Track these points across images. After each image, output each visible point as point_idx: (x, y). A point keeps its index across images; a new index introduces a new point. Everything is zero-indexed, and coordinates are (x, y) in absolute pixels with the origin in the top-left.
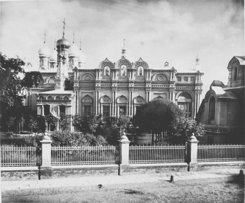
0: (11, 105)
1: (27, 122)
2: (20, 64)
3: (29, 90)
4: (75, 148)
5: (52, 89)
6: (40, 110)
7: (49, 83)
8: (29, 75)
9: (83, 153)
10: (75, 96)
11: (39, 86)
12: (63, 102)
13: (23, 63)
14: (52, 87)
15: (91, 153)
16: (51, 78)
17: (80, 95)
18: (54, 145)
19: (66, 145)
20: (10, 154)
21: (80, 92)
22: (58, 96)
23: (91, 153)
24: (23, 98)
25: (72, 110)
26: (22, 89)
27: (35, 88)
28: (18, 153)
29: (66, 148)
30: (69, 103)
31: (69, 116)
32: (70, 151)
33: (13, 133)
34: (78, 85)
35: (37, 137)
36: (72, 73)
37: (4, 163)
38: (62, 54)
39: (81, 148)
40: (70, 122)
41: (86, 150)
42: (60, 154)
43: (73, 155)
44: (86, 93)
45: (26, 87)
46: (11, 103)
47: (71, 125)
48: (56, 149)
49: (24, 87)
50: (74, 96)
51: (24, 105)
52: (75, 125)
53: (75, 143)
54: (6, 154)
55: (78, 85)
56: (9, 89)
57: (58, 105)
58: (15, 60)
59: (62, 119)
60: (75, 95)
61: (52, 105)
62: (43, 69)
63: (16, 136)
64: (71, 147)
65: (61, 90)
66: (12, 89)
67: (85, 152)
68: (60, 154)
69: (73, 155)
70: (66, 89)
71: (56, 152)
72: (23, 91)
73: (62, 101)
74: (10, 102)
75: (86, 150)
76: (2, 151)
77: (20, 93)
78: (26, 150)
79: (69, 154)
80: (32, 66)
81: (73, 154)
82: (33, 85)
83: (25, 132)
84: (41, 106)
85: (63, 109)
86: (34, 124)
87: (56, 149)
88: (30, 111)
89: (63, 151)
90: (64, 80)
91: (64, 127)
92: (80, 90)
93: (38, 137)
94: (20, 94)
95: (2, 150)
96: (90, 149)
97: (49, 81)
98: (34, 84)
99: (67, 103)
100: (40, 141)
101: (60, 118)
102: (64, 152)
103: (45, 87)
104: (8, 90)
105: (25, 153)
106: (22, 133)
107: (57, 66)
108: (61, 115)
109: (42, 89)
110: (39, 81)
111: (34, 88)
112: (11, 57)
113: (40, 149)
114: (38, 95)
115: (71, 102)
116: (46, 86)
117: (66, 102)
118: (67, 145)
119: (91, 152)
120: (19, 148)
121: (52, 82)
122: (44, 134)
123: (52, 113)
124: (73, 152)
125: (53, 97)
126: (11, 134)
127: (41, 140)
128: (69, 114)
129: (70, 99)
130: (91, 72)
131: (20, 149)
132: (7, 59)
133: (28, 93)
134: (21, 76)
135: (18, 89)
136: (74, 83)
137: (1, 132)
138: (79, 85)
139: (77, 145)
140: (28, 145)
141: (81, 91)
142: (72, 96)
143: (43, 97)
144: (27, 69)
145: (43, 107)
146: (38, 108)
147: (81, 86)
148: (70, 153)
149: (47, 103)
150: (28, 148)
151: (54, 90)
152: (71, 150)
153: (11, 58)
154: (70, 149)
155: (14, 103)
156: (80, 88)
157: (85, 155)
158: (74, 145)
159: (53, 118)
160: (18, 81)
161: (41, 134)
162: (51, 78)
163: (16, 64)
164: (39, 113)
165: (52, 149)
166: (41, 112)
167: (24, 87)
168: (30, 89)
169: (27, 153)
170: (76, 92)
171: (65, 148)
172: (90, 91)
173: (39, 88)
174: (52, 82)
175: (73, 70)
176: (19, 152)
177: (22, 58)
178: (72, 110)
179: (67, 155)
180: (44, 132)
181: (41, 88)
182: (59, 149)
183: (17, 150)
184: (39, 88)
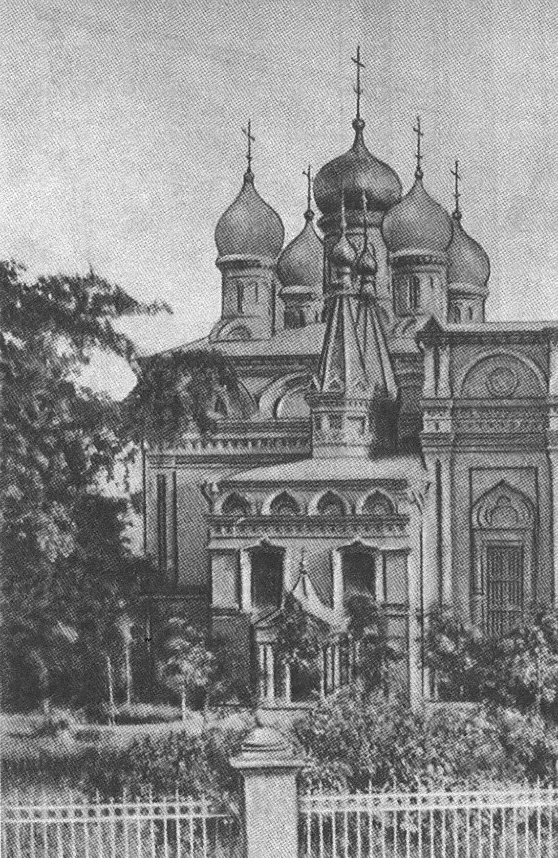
0: (60, 555)
1: (151, 657)
2: (106, 308)
3: (160, 461)
4: (434, 798)
5: (297, 449)
6: (231, 578)
7: (279, 415)
8: (157, 372)
9: (484, 826)
10: (433, 489)
11: (219, 436)
12: (359, 520)
13: (123, 303)
14: (299, 441)
15: (533, 827)
16: (289, 385)
17: (463, 482)
18: (315, 782)
19: (380, 779)
20: (60, 842)
21: (462, 467)
22: (334, 492)
23: (533, 827)
24: (131, 511)
25: (419, 576)
26: (125, 451)
27: (200, 451)
28: (105, 835)
29: (383, 797)
30: (398, 533)
31: (398, 606)
32: (407, 816)
33: (72, 721)
34: (446, 427)
35: (216, 736)
36: (412, 355)
37: (342, 814)
38: (352, 246)
39: (473, 799)
40: (405, 640)
41: (499, 810)
42: (353, 837)
43: (426, 840)
44: (498, 469)
45: (146, 445)
46: (56, 542)
47: (413, 660)
48: (323, 804)
49: (131, 444)
50: (428, 488)
51: (136, 548)
52: (436, 661)
53: (436, 771)
54: (32, 841)
55: (446, 427)
56: (42, 459)
57: (326, 545)
58: (77, 285)
59: (356, 626)
60: (429, 484)
61: (298, 552)
62: (244, 334)
63: (96, 736)
64: (413, 790)
65: (347, 457)
66: (62, 455)
67: (497, 819)
68: (353, 837)
69: (426, 840)
70: (377, 453)
71: (327, 826)
72: (130, 465)
73: (357, 523)
74: (50, 533)
75: (499, 810)
76: (9, 829)
77: (110, 477)
78: (152, 817)
79: (402, 834)
80: (169, 311)
81: (425, 831)
82: (186, 431)
83: (145, 709)
84: (234, 554)
85: (360, 565)
86: (192, 669)
87: (323, 804)
88: (163, 590)
89: (364, 815)
90: (371, 464)
91: (372, 665)
92: (460, 457)
93: (219, 741)
94: (112, 482)
95: (12, 821)
96: (526, 804)
97: (277, 403)
98: (192, 425)
99: (386, 533)
100: (235, 763)
101: (348, 620)
102: (374, 823)
103: (254, 442)
104: (39, 466)
105: (146, 834)
106: (124, 719)
107: (327, 315)
108: (350, 606)
109: (239, 451)
110: (220, 407)
111: (189, 450)
112: (50, 270)
113: (234, 807)
114: (215, 488)
115: (411, 529)
116: (264, 435)
117: (378, 528)
118: (392, 785)
119: (533, 819)
120: (111, 807)
121: (296, 407)
122: (252, 719)
123: (298, 594)
124: (426, 821)
125: (297, 496)
126: (63, 725)
127: (236, 751)
128: (394, 597)
129: (404, 508)
130: (522, 347)
131: (118, 812)
132: (27, 278)
133: (155, 481)
134: (107, 377)
135: (97, 461)
136: (426, 416)
137: (5, 711)
138: (456, 424)
139: (446, 779)
140: (162, 787)
141: (463, 462)
142: (415, 488)
143: (244, 505)
144: (152, 336)
145: (245, 559)
146: (218, 564)
147: (467, 430)
148: (408, 827)
149: (266, 536)
150: (164, 805)
151: (309, 456)
152: (412, 814)
153: (54, 273)
154: (408, 808)
155: (80, 540)
156: (456, 443)
157: (495, 836)
158: (430, 782)
159: (302, 625)
160: (91, 413)
161: (235, 721)
162: (289, 385)
163: (81, 307)
164: (221, 598)
165: (10, 814)
166: (231, 589)
167: (131, 444)
168: (171, 452)
169: (159, 835)
170: (438, 466)
171: (377, 803)
172: (515, 460)
173: (220, 449)
174: (296, 407)
175: (418, 337)
176: (113, 830)
177: (118, 275)
178: (419, 576)
179: (389, 837)
180: (249, 700)
181: (235, 443)
182: (347, 810)
183: (99, 819)
184: (220, 446)
